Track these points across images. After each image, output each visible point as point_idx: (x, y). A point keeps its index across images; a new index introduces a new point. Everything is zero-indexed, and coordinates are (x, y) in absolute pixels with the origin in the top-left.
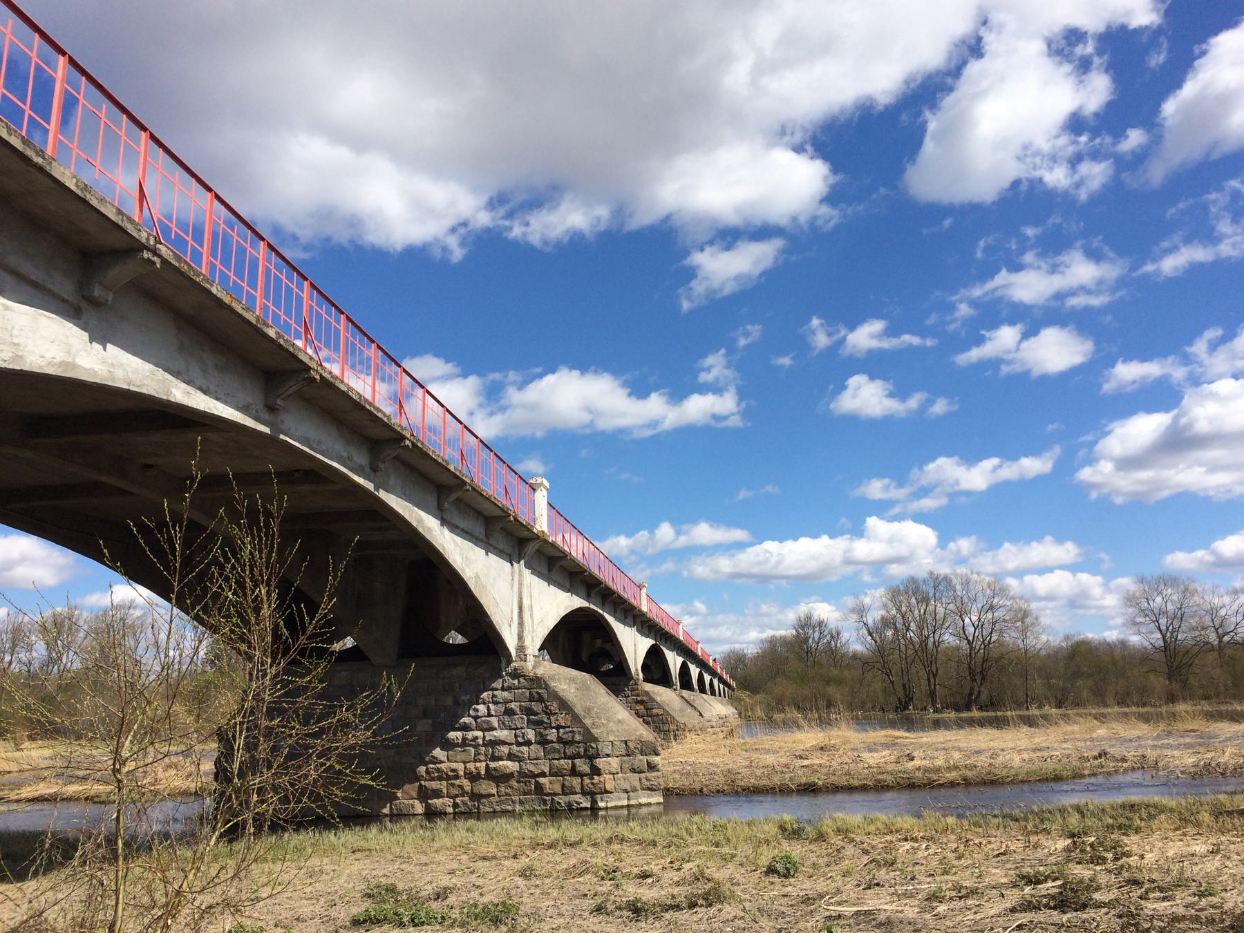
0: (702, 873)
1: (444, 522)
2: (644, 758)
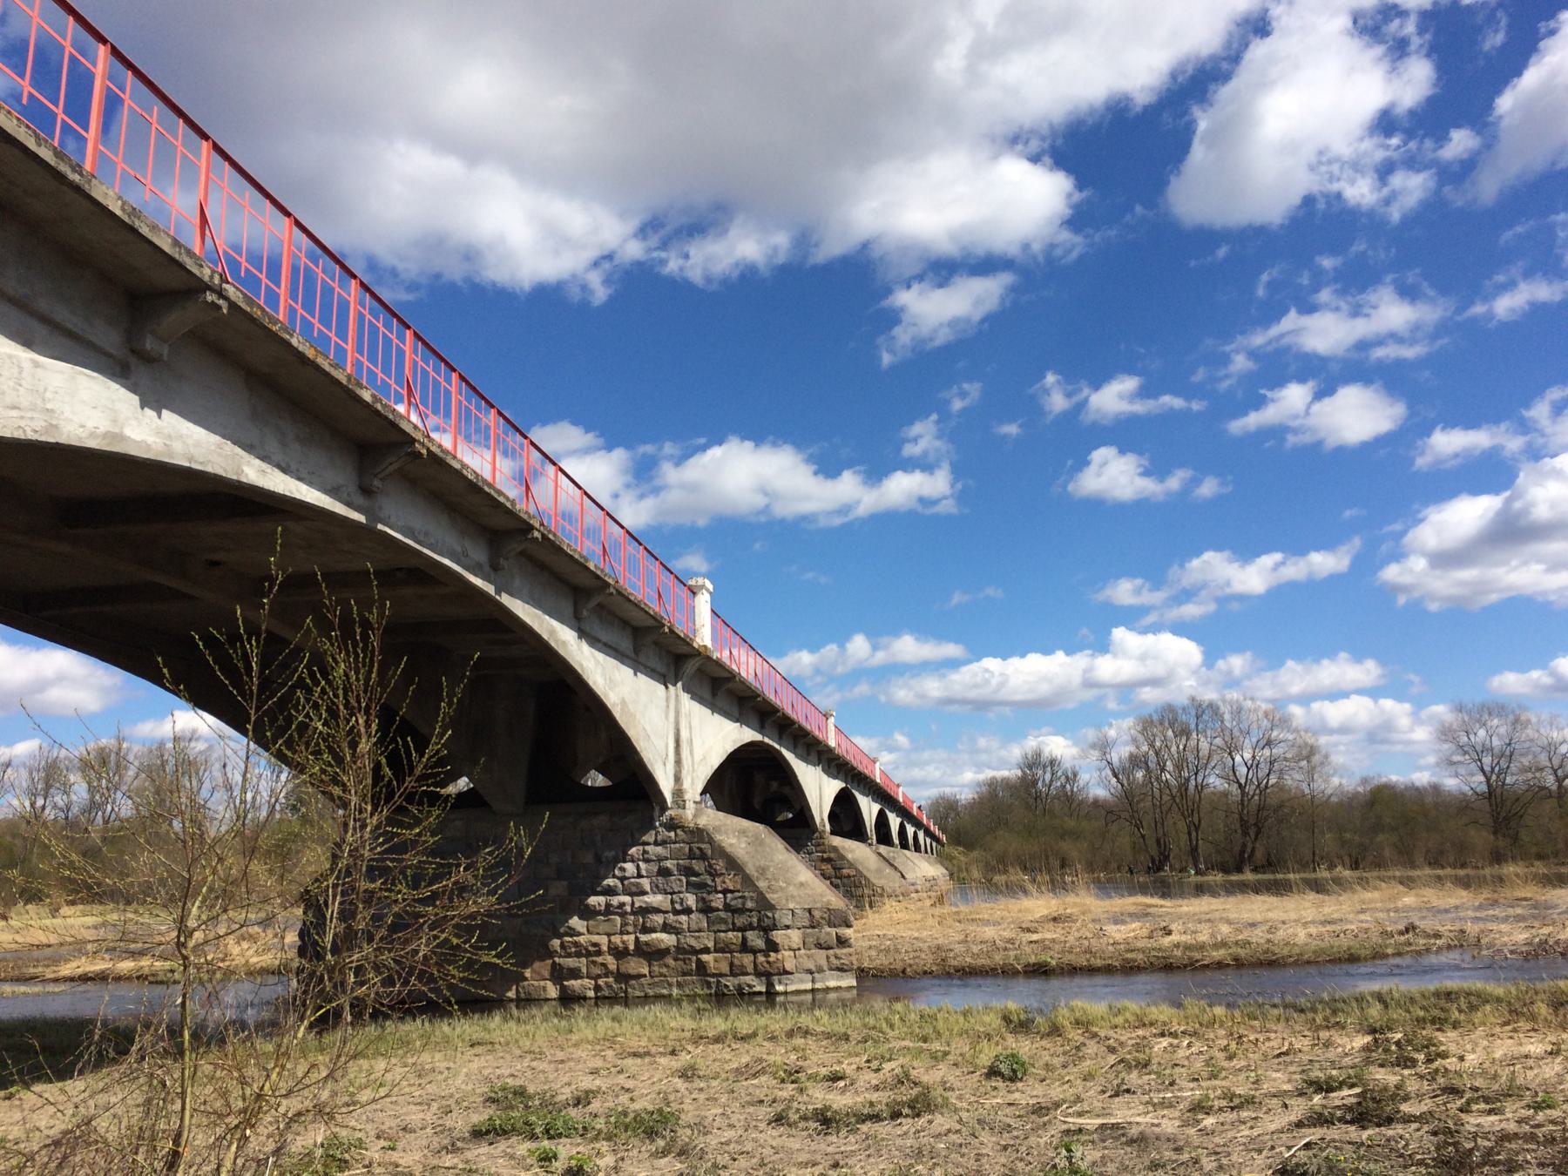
0: (907, 1075)
1: (583, 634)
2: (833, 931)
